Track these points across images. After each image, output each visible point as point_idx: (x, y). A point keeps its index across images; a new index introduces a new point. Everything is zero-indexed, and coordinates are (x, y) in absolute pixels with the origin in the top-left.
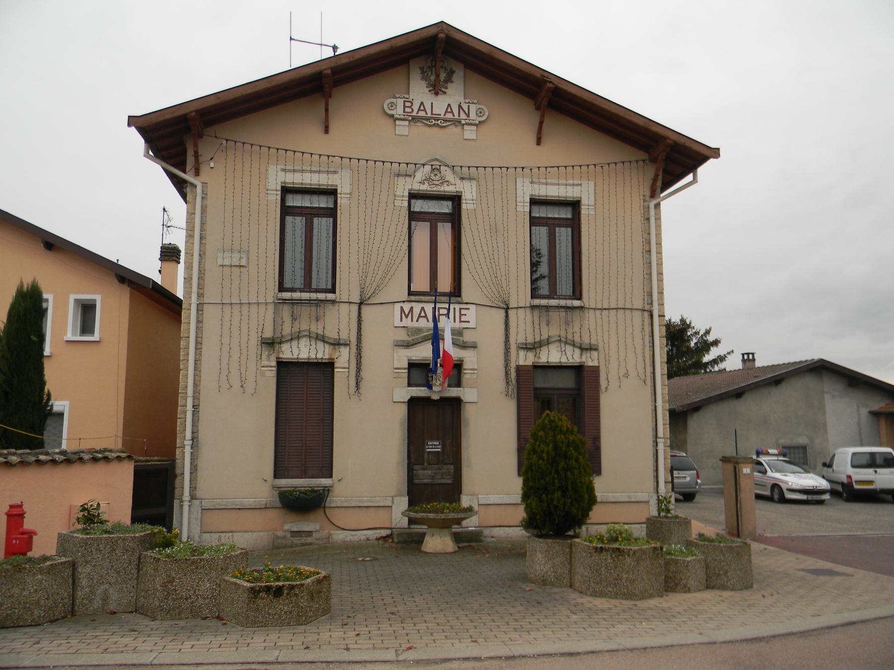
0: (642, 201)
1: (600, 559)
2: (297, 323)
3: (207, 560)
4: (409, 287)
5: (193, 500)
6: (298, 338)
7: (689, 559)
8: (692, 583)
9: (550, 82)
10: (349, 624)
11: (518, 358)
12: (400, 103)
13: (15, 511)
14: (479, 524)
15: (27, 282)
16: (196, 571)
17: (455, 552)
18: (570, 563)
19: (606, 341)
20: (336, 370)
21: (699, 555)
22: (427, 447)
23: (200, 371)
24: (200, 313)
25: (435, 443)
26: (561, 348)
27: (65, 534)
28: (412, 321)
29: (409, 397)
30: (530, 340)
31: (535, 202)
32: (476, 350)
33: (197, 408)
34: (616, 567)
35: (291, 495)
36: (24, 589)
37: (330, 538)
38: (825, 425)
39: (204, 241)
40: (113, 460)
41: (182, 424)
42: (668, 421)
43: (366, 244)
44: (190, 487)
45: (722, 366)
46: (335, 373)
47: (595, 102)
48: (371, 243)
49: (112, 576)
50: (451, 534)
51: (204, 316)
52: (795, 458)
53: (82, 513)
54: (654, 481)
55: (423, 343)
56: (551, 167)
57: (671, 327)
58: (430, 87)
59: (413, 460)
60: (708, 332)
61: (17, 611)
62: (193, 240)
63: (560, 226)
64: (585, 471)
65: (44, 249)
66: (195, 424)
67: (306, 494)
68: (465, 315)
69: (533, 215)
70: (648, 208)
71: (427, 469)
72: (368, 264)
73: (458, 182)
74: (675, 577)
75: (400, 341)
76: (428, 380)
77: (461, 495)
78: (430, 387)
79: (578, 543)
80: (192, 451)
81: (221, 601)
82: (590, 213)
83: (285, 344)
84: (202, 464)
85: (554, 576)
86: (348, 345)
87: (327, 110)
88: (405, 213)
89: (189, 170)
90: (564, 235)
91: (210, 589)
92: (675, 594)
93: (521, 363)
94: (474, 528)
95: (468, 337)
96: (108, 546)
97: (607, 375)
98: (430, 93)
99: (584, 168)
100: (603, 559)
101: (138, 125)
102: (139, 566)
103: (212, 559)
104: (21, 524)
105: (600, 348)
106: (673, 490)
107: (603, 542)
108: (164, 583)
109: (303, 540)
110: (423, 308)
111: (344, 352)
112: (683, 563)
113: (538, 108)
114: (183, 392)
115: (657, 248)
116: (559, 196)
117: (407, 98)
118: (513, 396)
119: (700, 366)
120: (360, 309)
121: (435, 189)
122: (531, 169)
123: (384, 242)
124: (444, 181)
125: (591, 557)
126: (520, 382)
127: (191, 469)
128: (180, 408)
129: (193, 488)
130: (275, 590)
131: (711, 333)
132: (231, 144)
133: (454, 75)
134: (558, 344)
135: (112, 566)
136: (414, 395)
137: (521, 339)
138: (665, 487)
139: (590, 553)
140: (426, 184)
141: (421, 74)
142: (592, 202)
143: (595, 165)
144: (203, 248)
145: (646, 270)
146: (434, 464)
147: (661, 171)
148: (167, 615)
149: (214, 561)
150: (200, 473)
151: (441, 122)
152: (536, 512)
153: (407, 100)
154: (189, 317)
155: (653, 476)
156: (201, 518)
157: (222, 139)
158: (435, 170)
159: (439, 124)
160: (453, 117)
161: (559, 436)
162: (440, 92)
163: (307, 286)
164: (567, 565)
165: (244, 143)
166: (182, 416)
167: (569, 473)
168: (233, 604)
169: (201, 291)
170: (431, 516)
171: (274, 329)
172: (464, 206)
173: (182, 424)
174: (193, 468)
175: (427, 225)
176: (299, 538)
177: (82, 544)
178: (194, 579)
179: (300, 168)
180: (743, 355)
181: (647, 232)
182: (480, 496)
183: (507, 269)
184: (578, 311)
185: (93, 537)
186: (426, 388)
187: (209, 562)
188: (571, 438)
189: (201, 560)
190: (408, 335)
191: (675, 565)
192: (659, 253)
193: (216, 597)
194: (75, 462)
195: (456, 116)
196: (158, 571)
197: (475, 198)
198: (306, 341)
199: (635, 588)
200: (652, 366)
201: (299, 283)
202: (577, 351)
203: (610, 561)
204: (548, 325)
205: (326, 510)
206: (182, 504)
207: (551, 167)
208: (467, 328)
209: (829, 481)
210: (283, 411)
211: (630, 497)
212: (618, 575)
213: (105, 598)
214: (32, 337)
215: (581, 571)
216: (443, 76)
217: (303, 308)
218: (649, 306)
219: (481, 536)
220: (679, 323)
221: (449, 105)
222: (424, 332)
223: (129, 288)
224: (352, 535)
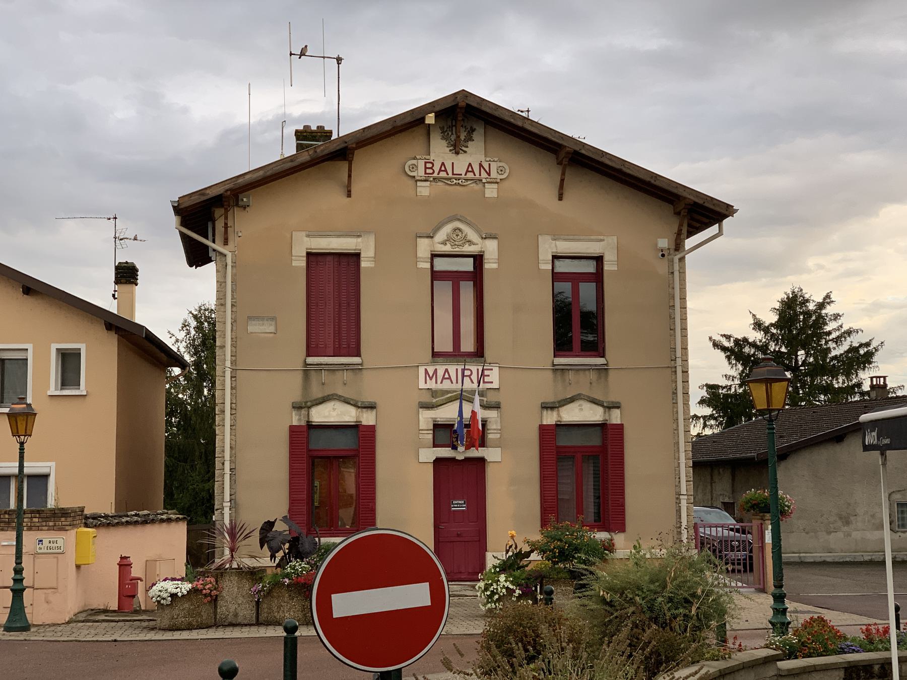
22: (452, 506)
25: (460, 502)
28: (436, 383)
68: (489, 376)
110: (447, 370)
121: (457, 249)
151: (462, 181)
159: (460, 183)
221: (470, 165)
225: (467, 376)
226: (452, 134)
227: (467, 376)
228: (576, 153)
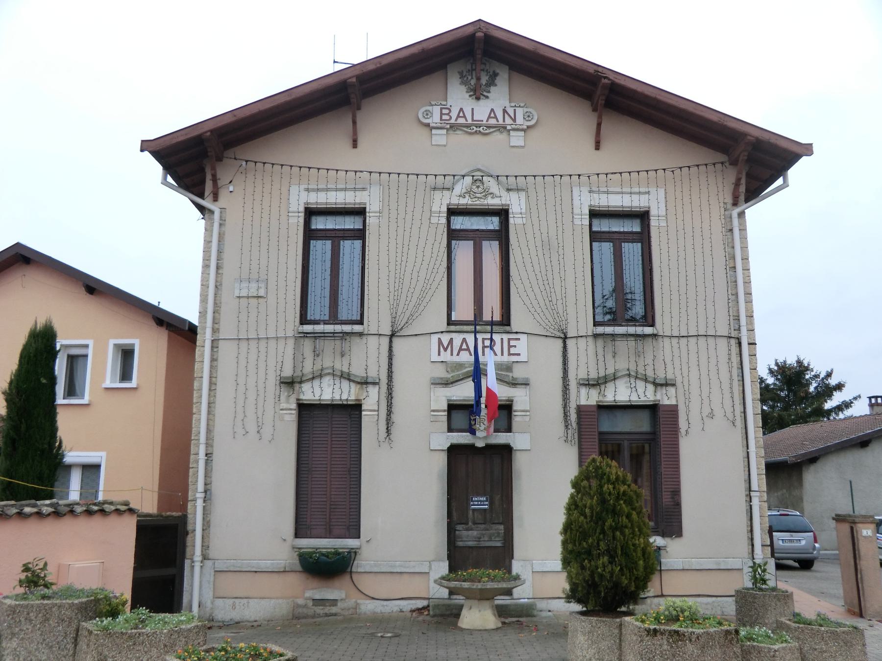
0: (722, 210)
1: (654, 645)
2: (319, 360)
3: (147, 635)
4: (449, 315)
5: (205, 561)
6: (321, 376)
7: (776, 647)
9: (605, 78)
11: (578, 396)
12: (436, 110)
15: (41, 323)
16: (133, 648)
17: (497, 629)
18: (620, 647)
19: (685, 374)
20: (363, 413)
22: (472, 503)
23: (214, 415)
24: (215, 350)
26: (631, 384)
28: (452, 355)
29: (449, 445)
30: (593, 375)
32: (528, 387)
34: (674, 656)
35: (311, 558)
39: (220, 271)
40: (110, 513)
42: (764, 471)
43: (398, 267)
44: (202, 546)
45: (848, 412)
46: (363, 417)
47: (659, 97)
49: (43, 653)
50: (493, 606)
51: (219, 354)
53: (25, 574)
54: (748, 544)
56: (612, 173)
57: (786, 370)
58: (471, 91)
59: (455, 517)
60: (829, 375)
62: (209, 271)
64: (640, 530)
65: (86, 293)
66: (207, 475)
67: (327, 557)
68: (515, 346)
69: (595, 229)
70: (731, 217)
71: (472, 530)
72: (400, 290)
73: (504, 193)
75: (438, 378)
76: (470, 423)
78: (473, 432)
83: (306, 384)
84: (216, 518)
87: (354, 123)
90: (632, 251)
93: (583, 402)
94: (526, 600)
95: (518, 373)
96: (40, 615)
97: (688, 415)
98: (471, 98)
100: (657, 644)
101: (151, 149)
103: (154, 633)
105: (679, 383)
107: (660, 623)
110: (464, 340)
111: (373, 391)
112: (769, 652)
114: (196, 438)
115: (743, 264)
118: (573, 441)
119: (820, 413)
120: (391, 342)
121: (478, 202)
122: (589, 177)
123: (418, 265)
124: (487, 193)
125: (642, 641)
126: (581, 425)
127: (203, 525)
128: (192, 457)
129: (205, 547)
131: (833, 375)
132: (251, 164)
133: (498, 78)
134: (627, 379)
135: (44, 640)
136: (455, 441)
137: (583, 375)
138: (762, 551)
140: (467, 197)
141: (460, 78)
142: (662, 212)
143: (664, 170)
144: (219, 279)
146: (481, 524)
147: (744, 174)
149: (155, 636)
150: (213, 530)
151: (483, 129)
152: (577, 581)
154: (202, 355)
155: (746, 538)
156: (214, 581)
157: (241, 160)
158: (477, 182)
159: (482, 130)
160: (496, 123)
161: (606, 486)
162: (482, 97)
163: (334, 319)
164: (616, 651)
165: (264, 163)
166: (194, 465)
167: (618, 533)
170: (466, 585)
171: (294, 367)
172: (511, 221)
174: (206, 524)
175: (471, 243)
176: (322, 607)
180: (870, 398)
181: (730, 245)
182: (534, 562)
183: (564, 291)
184: (650, 339)
185: (23, 604)
187: (149, 637)
188: (622, 489)
189: (139, 634)
190: (448, 372)
192: (746, 269)
194: (65, 515)
195: (501, 122)
197: (524, 211)
198: (329, 380)
200: (742, 404)
202: (651, 387)
203: (666, 647)
204: (614, 357)
207: (612, 173)
208: (517, 362)
210: (305, 457)
211: (718, 563)
214: (42, 379)
216: (484, 80)
220: (795, 365)
221: (492, 110)
222: (466, 368)
223: (167, 331)
224: (383, 606)
225: (487, 347)
226: (472, 78)
227: (487, 347)
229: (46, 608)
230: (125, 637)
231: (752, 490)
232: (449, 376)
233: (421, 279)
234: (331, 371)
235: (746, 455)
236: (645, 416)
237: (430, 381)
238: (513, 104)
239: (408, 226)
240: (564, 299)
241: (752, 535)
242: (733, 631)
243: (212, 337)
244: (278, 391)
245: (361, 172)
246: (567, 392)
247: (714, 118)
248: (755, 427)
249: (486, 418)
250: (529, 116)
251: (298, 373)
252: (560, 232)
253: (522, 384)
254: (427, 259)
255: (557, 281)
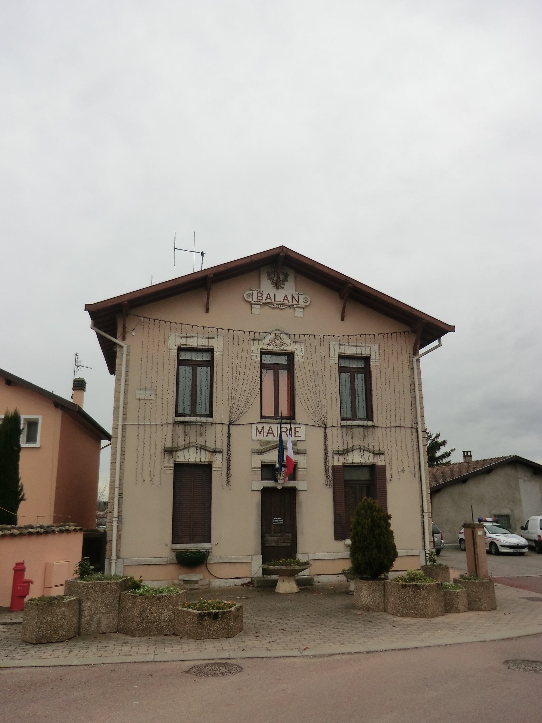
0: (408, 357)
2: (187, 437)
6: (189, 447)
7: (458, 591)
8: (461, 607)
9: (350, 283)
10: (260, 636)
11: (333, 460)
12: (255, 294)
13: (20, 567)
14: (309, 572)
15: (11, 411)
17: (298, 592)
18: (384, 596)
19: (389, 448)
20: (213, 469)
21: (463, 588)
22: (274, 521)
24: (124, 431)
25: (279, 518)
27: (71, 581)
28: (263, 436)
30: (341, 448)
31: (341, 357)
32: (306, 455)
33: (121, 495)
34: (415, 597)
36: (54, 617)
37: (210, 584)
38: (520, 501)
39: (127, 383)
41: (111, 506)
43: (233, 385)
45: (448, 459)
48: (236, 384)
50: (295, 579)
52: (502, 523)
55: (270, 451)
56: (351, 335)
60: (438, 436)
61: (49, 632)
63: (358, 373)
67: (195, 554)
68: (298, 432)
70: (412, 361)
72: (235, 398)
73: (292, 344)
74: (450, 603)
77: (297, 554)
78: (276, 481)
79: (389, 582)
80: (118, 525)
81: (176, 623)
82: (377, 365)
84: (124, 534)
85: (374, 605)
86: (222, 452)
87: (208, 299)
88: (258, 364)
89: (119, 336)
90: (360, 378)
91: (168, 616)
92: (450, 614)
93: (336, 463)
94: (306, 576)
95: (300, 447)
97: (391, 471)
99: (372, 336)
102: (119, 602)
103: (170, 596)
104: (23, 576)
105: (386, 453)
106: (434, 547)
107: (406, 582)
108: (141, 612)
109: (192, 586)
110: (270, 428)
111: (219, 456)
112: (455, 593)
113: (342, 298)
116: (357, 354)
117: (259, 291)
120: (229, 428)
121: (277, 349)
122: (339, 336)
124: (283, 344)
125: (399, 591)
127: (117, 537)
129: (118, 551)
130: (214, 615)
134: (359, 450)
135: (104, 602)
136: (265, 486)
137: (335, 448)
139: (399, 588)
142: (377, 358)
145: (413, 402)
148: (142, 633)
149: (171, 597)
150: (122, 540)
151: (280, 306)
153: (259, 292)
156: (123, 572)
157: (140, 316)
158: (277, 337)
160: (288, 303)
162: (280, 287)
163: (193, 413)
164: (382, 597)
165: (155, 320)
167: (382, 538)
168: (185, 625)
169: (125, 416)
170: (284, 568)
173: (111, 506)
176: (189, 585)
177: (85, 587)
178: (159, 609)
179: (190, 335)
180: (464, 452)
181: (412, 377)
184: (371, 429)
186: (274, 481)
191: (449, 595)
192: (421, 390)
193: (172, 621)
196: (135, 604)
197: (303, 354)
198: (193, 450)
199: (428, 610)
201: (188, 410)
205: (207, 565)
206: (111, 561)
207: (351, 335)
209: (527, 539)
211: (407, 553)
212: (417, 602)
213: (99, 623)
214: (15, 447)
215: (392, 600)
217: (192, 427)
218: (415, 425)
219: (312, 581)
221: (286, 296)
222: (271, 443)
223: (61, 411)
224: (225, 583)
228: (215, 275)
229: (104, 585)
230: (155, 598)
231: (424, 511)
232: (262, 448)
233: (247, 392)
234: (194, 445)
235: (421, 493)
236: (366, 471)
237: (252, 450)
238: (297, 293)
239: (239, 361)
240: (325, 405)
241: (424, 536)
242: (440, 584)
243: (123, 423)
244: (163, 456)
245: (212, 328)
246: (327, 458)
247: (407, 309)
248: (425, 477)
249: (284, 473)
250: (306, 300)
251: (175, 446)
252: (323, 368)
253: (302, 453)
254: (250, 381)
255: (322, 395)
